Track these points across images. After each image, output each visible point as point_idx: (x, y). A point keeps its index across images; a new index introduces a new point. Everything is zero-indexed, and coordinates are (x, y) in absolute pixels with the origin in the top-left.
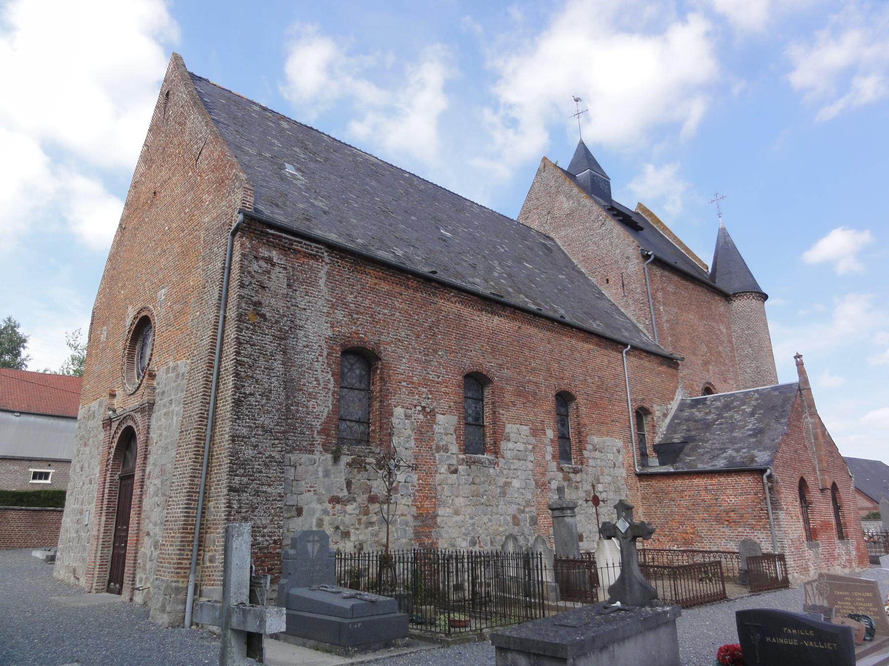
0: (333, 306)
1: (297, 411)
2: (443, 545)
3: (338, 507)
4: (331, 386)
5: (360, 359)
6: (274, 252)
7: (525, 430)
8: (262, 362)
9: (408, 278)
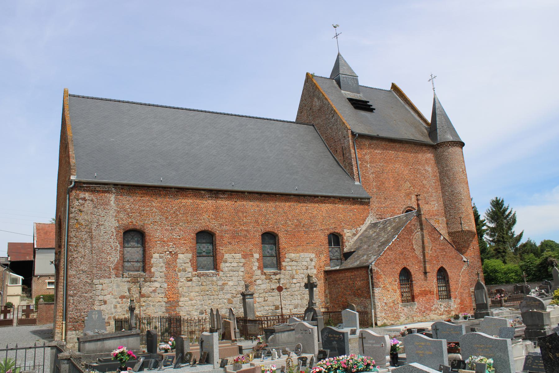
0: (118, 212)
1: (102, 261)
2: (183, 314)
3: (124, 300)
4: (118, 249)
5: (134, 235)
6: (87, 194)
7: (239, 256)
8: (81, 244)
9: (160, 191)
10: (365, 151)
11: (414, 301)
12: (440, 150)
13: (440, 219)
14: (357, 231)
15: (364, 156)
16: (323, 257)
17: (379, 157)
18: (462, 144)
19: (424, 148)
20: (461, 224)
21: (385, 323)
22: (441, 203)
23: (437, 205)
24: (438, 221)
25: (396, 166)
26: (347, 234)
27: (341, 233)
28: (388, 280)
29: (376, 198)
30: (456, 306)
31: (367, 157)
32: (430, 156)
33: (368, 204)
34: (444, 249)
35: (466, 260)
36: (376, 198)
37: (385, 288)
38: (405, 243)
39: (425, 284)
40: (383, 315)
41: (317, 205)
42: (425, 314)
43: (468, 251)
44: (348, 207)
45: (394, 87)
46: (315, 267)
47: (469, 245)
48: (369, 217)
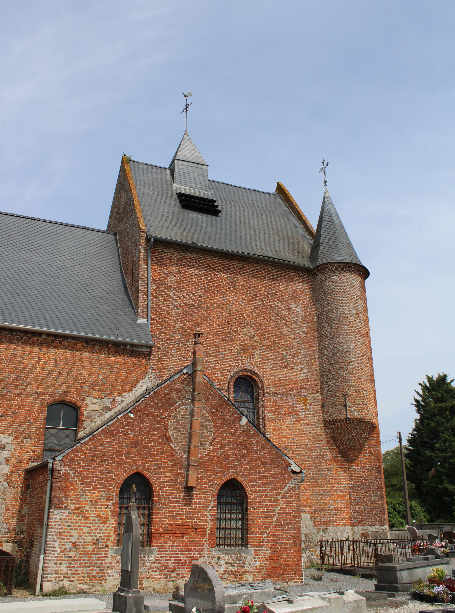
10: (170, 269)
11: (150, 545)
12: (320, 277)
13: (310, 396)
14: (114, 404)
15: (166, 276)
16: (28, 445)
17: (196, 280)
18: (364, 273)
19: (291, 274)
20: (346, 406)
21: (63, 587)
22: (316, 368)
23: (305, 370)
24: (306, 400)
25: (230, 298)
26: (92, 407)
27: (79, 404)
28: (90, 495)
29: (178, 350)
30: (258, 563)
31: (172, 280)
32: (302, 287)
33: (147, 355)
34: (245, 444)
35: (298, 470)
36: (178, 350)
37: (79, 511)
38: (147, 424)
39: (185, 510)
40: (63, 568)
41: (36, 349)
42: (174, 575)
43: (361, 458)
44: (105, 357)
45: (280, 189)
46: (7, 460)
47: (362, 446)
48: (146, 380)
